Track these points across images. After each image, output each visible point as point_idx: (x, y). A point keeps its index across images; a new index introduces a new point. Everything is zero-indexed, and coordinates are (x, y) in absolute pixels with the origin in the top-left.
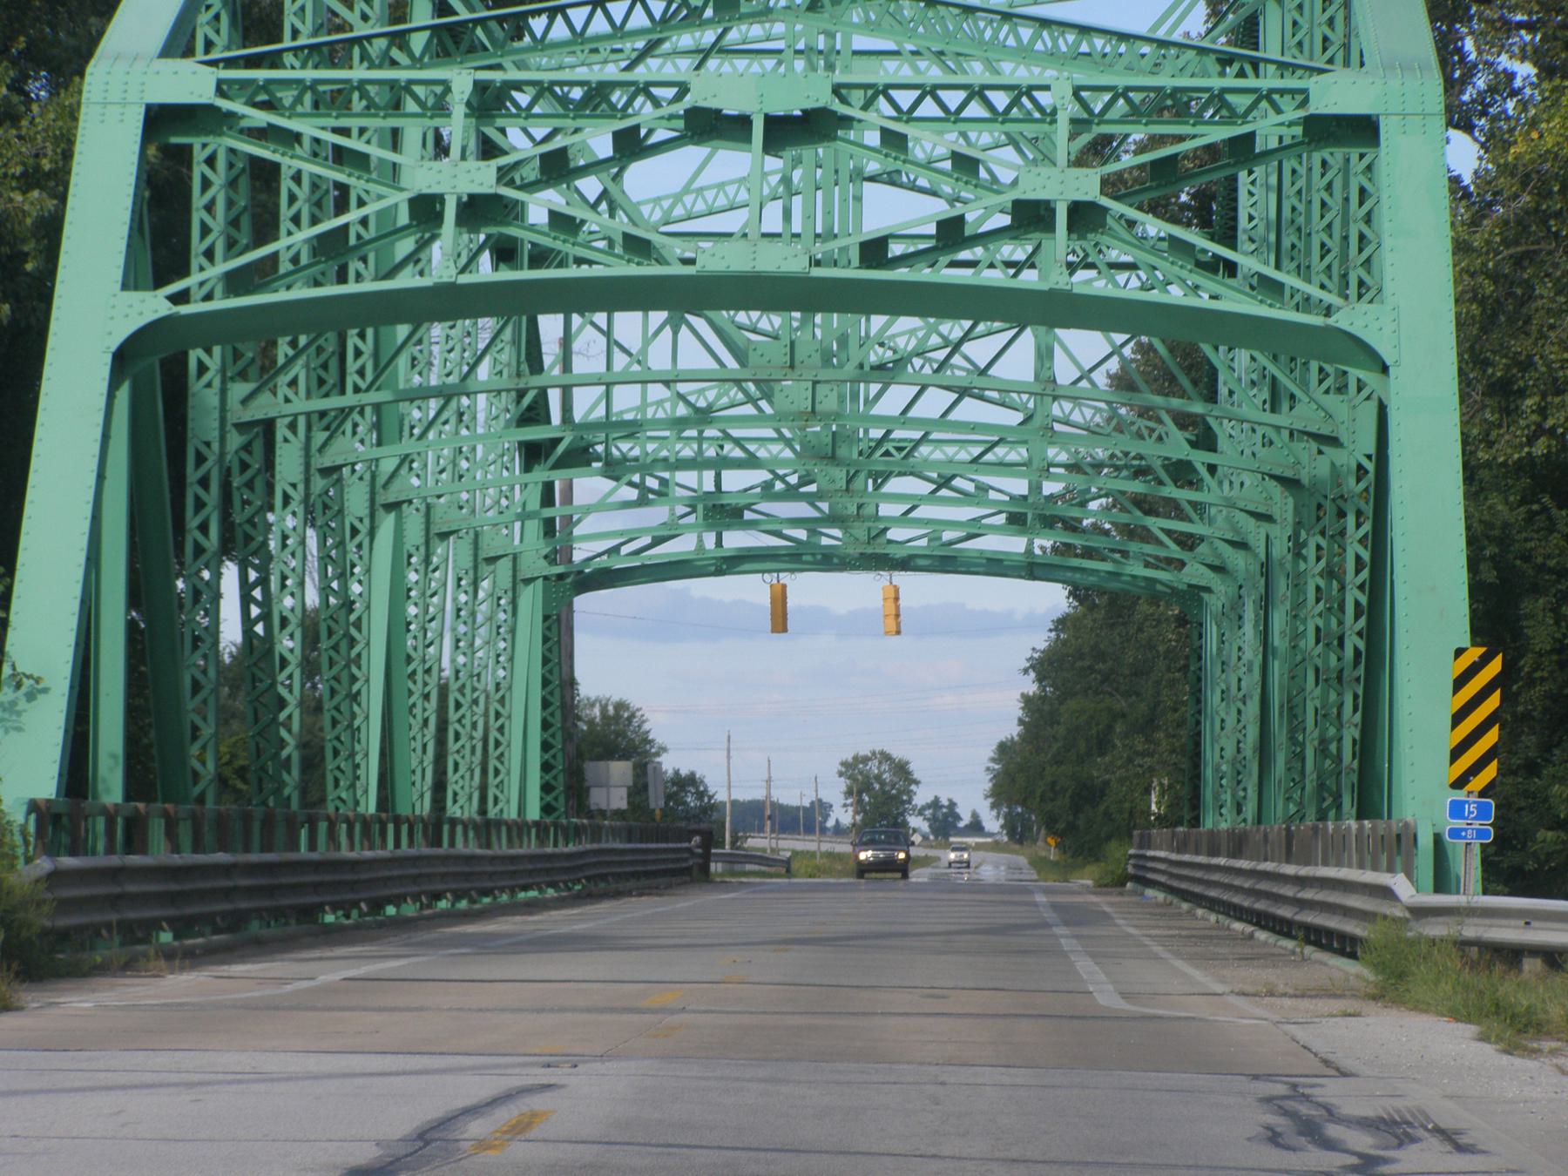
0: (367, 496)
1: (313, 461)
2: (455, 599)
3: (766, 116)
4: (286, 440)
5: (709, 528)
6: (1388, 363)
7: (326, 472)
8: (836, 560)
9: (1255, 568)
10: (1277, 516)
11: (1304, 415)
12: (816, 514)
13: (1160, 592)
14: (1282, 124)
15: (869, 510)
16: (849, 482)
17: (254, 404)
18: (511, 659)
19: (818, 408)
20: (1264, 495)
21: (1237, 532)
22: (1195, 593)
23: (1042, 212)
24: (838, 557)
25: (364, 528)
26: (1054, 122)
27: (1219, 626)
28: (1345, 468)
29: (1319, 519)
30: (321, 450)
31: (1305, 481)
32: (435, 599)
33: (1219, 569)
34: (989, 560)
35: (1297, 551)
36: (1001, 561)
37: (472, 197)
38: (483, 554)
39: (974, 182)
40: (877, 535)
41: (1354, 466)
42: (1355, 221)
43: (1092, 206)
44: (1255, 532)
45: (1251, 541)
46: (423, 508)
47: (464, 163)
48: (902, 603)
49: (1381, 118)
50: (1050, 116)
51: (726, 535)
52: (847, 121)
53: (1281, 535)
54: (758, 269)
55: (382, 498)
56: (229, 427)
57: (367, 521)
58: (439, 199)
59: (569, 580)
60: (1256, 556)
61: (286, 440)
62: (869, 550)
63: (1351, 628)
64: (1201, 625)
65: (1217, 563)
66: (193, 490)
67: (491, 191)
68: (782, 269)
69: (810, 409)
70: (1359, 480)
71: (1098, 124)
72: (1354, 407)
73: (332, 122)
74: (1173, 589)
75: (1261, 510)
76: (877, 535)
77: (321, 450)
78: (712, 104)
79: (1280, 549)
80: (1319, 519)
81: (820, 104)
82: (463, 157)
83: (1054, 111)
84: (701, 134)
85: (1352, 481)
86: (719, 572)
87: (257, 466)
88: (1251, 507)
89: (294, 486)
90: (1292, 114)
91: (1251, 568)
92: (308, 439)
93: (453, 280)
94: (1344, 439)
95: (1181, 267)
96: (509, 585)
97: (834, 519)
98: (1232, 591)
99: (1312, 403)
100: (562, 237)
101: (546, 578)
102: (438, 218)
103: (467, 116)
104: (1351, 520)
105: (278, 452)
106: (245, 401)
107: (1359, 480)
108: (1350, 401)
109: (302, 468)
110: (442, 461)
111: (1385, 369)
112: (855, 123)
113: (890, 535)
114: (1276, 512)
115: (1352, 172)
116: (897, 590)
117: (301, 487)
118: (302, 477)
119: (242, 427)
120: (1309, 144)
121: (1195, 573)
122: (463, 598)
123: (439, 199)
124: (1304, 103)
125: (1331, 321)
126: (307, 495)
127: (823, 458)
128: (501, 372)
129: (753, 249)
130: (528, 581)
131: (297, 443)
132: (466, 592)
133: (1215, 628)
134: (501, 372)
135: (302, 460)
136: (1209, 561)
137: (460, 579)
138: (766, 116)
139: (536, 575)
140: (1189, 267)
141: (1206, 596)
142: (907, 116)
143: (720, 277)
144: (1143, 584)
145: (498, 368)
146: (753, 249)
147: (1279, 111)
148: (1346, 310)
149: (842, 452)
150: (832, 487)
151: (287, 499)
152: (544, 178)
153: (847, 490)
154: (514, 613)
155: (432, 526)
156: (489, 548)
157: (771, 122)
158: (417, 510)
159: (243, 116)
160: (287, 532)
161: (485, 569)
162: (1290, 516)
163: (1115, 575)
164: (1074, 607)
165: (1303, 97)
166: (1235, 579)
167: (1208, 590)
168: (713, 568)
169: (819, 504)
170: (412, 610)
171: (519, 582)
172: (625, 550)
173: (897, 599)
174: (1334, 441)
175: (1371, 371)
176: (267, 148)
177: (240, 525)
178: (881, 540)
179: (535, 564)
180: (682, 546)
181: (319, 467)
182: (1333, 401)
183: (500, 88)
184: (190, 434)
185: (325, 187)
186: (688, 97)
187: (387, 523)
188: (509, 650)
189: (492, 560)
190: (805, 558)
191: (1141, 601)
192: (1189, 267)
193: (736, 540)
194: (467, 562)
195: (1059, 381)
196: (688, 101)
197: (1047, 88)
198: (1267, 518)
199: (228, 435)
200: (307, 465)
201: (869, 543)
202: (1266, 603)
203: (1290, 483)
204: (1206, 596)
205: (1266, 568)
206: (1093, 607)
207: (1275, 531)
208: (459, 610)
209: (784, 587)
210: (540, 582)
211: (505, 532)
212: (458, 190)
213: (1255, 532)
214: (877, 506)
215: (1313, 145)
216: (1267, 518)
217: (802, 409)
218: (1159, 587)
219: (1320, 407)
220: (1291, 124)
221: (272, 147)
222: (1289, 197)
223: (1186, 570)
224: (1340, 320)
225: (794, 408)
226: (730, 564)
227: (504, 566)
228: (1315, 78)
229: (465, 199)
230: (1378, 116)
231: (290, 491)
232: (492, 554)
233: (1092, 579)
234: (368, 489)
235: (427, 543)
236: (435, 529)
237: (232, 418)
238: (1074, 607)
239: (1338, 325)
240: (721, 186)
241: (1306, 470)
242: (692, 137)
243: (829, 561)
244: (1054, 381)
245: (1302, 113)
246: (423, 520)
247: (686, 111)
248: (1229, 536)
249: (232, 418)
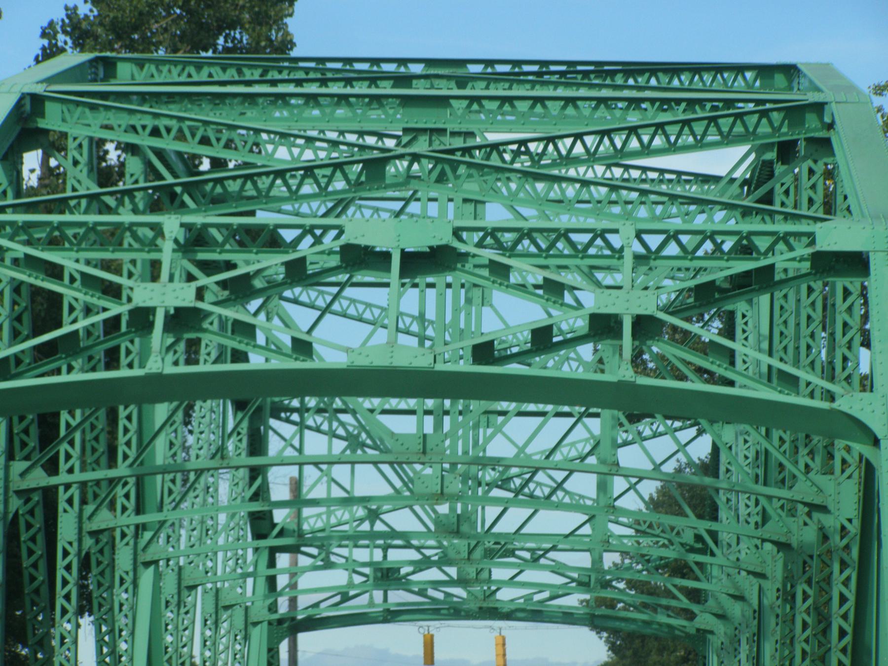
0: (132, 557)
1: (84, 526)
2: (203, 634)
3: (403, 251)
4: (65, 511)
5: (376, 586)
6: (879, 437)
7: (95, 534)
8: (463, 613)
9: (749, 613)
10: (769, 575)
11: (803, 490)
12: (444, 578)
13: (678, 636)
14: (794, 259)
15: (485, 575)
16: (470, 553)
17: (29, 476)
18: (132, 633)
19: (446, 491)
20: (760, 560)
21: (737, 588)
22: (703, 634)
23: (612, 324)
24: (464, 611)
25: (129, 579)
26: (621, 257)
27: (718, 656)
28: (832, 529)
29: (804, 572)
30: (90, 518)
31: (795, 544)
32: (187, 632)
33: (721, 617)
34: (565, 613)
35: (789, 597)
36: (572, 614)
37: (177, 309)
38: (185, 583)
39: (560, 302)
40: (489, 596)
41: (839, 527)
42: (840, 347)
43: (651, 319)
44: (750, 587)
45: (747, 595)
46: (176, 569)
47: (171, 284)
48: (508, 657)
49: (871, 254)
50: (618, 253)
51: (390, 593)
52: (464, 257)
53: (771, 588)
54: (394, 364)
55: (142, 558)
56: (11, 493)
57: (131, 574)
58: (151, 311)
59: (286, 625)
60: (750, 605)
61: (65, 511)
62: (485, 605)
63: (836, 647)
64: (705, 657)
65: (720, 612)
66: (60, 572)
67: (192, 305)
68: (413, 365)
69: (439, 492)
70: (842, 538)
71: (655, 259)
72: (839, 484)
73: (74, 255)
74: (686, 633)
75: (758, 570)
76: (489, 596)
77: (90, 518)
78: (362, 242)
79: (770, 597)
80: (804, 572)
81: (443, 242)
82: (171, 279)
83: (622, 249)
84: (353, 266)
85: (838, 538)
86: (385, 621)
87: (38, 526)
88: (751, 568)
89: (70, 544)
90: (802, 250)
91: (747, 614)
92: (81, 511)
93: (160, 371)
94: (831, 507)
95: (719, 366)
96: (242, 627)
97: (461, 582)
98: (730, 631)
99: (808, 481)
100: (246, 341)
101: (270, 623)
102: (150, 326)
103: (174, 251)
104: (836, 567)
105: (60, 519)
106: (23, 475)
107: (842, 538)
108: (836, 479)
109: (76, 531)
110: (192, 539)
111: (876, 442)
112: (470, 258)
113: (500, 595)
114: (768, 572)
115: (837, 311)
116: (504, 639)
117: (75, 545)
118: (76, 537)
119: (19, 493)
120: (815, 274)
121: (704, 620)
122: (208, 633)
123: (151, 311)
124: (813, 243)
125: (835, 405)
126: (80, 551)
127: (451, 533)
128: (237, 484)
129: (391, 349)
130: (255, 624)
131: (73, 512)
132: (210, 629)
133: (715, 658)
134: (237, 484)
135: (76, 525)
136: (714, 611)
137: (206, 621)
138: (403, 251)
139: (261, 619)
140: (725, 366)
141: (709, 636)
142: (511, 251)
143: (367, 370)
144: (666, 630)
145: (236, 481)
146: (391, 349)
147: (791, 249)
148: (846, 397)
149: (465, 528)
150: (458, 557)
151: (122, 581)
152: (233, 297)
153: (469, 559)
154: (135, 594)
155: (182, 582)
156: (224, 601)
157: (405, 256)
158: (173, 570)
159: (8, 249)
160: (122, 602)
161: (224, 616)
162: (779, 574)
163: (647, 623)
164: (612, 658)
165: (811, 238)
166: (733, 623)
167: (712, 632)
168: (381, 618)
169: (446, 569)
170: (169, 639)
171: (249, 624)
172: (323, 605)
173: (504, 644)
174: (824, 509)
175: (864, 444)
176: (24, 273)
177: (26, 568)
178: (492, 598)
179: (260, 611)
180: (358, 604)
181: (89, 530)
182: (822, 480)
183: (201, 229)
184: (59, 537)
185: (97, 334)
186: (343, 237)
187: (147, 577)
188: (130, 625)
189: (227, 608)
190: (443, 612)
191: (652, 653)
192: (725, 366)
193: (397, 597)
194: (211, 609)
195: (621, 465)
196: (343, 240)
197: (616, 231)
198: (762, 576)
199: (84, 539)
200: (80, 529)
201: (484, 600)
202: (758, 637)
203: (783, 546)
204: (709, 636)
205: (759, 613)
206: (623, 657)
207: (766, 585)
208: (205, 641)
209: (432, 636)
210: (265, 624)
211: (239, 590)
212: (166, 304)
213: (750, 587)
214: (490, 572)
215: (818, 275)
216: (762, 576)
217: (434, 492)
218: (677, 632)
219: (813, 484)
220: (802, 259)
221: (28, 272)
222: (778, 351)
223: (697, 619)
224: (843, 404)
225: (428, 491)
226: (390, 616)
227: (239, 613)
228: (819, 225)
229: (172, 312)
230: (868, 253)
231: (124, 576)
232: (227, 604)
233: (633, 627)
234: (132, 551)
235: (217, 613)
236: (185, 583)
237: (13, 487)
238: (612, 658)
239: (841, 408)
240: (368, 305)
241: (796, 537)
242: (346, 268)
243: (456, 612)
244: (618, 464)
245: (810, 250)
246: (176, 577)
247: (342, 247)
248: (731, 592)
249: (13, 487)
